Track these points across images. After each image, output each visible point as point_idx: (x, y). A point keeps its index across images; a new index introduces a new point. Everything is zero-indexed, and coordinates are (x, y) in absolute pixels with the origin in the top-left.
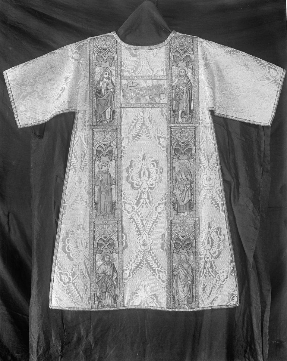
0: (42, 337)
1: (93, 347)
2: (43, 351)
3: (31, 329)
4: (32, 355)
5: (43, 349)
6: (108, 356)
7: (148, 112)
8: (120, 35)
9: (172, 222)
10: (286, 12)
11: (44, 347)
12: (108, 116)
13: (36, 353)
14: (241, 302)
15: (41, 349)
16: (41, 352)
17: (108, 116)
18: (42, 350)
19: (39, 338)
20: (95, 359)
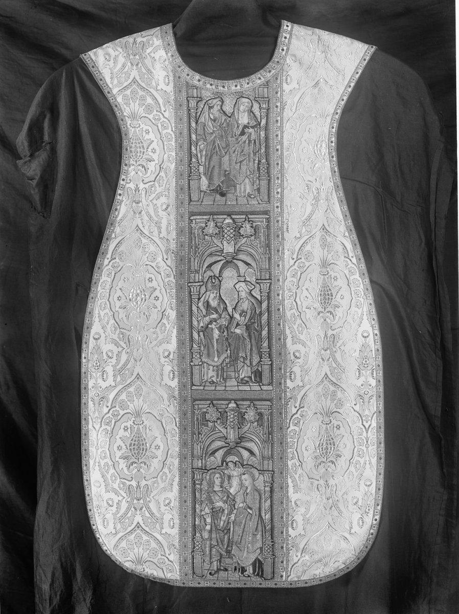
0: (59, 574)
1: (148, 587)
2: (60, 598)
3: (38, 560)
4: (40, 605)
5: (60, 595)
6: (176, 603)
7: (147, 55)
8: (177, 36)
9: (270, 360)
10: (457, 216)
11: (62, 591)
12: (375, 373)
13: (48, 601)
14: (450, 188)
15: (56, 595)
16: (56, 601)
17: (375, 373)
18: (58, 597)
19: (53, 575)
20: (153, 610)
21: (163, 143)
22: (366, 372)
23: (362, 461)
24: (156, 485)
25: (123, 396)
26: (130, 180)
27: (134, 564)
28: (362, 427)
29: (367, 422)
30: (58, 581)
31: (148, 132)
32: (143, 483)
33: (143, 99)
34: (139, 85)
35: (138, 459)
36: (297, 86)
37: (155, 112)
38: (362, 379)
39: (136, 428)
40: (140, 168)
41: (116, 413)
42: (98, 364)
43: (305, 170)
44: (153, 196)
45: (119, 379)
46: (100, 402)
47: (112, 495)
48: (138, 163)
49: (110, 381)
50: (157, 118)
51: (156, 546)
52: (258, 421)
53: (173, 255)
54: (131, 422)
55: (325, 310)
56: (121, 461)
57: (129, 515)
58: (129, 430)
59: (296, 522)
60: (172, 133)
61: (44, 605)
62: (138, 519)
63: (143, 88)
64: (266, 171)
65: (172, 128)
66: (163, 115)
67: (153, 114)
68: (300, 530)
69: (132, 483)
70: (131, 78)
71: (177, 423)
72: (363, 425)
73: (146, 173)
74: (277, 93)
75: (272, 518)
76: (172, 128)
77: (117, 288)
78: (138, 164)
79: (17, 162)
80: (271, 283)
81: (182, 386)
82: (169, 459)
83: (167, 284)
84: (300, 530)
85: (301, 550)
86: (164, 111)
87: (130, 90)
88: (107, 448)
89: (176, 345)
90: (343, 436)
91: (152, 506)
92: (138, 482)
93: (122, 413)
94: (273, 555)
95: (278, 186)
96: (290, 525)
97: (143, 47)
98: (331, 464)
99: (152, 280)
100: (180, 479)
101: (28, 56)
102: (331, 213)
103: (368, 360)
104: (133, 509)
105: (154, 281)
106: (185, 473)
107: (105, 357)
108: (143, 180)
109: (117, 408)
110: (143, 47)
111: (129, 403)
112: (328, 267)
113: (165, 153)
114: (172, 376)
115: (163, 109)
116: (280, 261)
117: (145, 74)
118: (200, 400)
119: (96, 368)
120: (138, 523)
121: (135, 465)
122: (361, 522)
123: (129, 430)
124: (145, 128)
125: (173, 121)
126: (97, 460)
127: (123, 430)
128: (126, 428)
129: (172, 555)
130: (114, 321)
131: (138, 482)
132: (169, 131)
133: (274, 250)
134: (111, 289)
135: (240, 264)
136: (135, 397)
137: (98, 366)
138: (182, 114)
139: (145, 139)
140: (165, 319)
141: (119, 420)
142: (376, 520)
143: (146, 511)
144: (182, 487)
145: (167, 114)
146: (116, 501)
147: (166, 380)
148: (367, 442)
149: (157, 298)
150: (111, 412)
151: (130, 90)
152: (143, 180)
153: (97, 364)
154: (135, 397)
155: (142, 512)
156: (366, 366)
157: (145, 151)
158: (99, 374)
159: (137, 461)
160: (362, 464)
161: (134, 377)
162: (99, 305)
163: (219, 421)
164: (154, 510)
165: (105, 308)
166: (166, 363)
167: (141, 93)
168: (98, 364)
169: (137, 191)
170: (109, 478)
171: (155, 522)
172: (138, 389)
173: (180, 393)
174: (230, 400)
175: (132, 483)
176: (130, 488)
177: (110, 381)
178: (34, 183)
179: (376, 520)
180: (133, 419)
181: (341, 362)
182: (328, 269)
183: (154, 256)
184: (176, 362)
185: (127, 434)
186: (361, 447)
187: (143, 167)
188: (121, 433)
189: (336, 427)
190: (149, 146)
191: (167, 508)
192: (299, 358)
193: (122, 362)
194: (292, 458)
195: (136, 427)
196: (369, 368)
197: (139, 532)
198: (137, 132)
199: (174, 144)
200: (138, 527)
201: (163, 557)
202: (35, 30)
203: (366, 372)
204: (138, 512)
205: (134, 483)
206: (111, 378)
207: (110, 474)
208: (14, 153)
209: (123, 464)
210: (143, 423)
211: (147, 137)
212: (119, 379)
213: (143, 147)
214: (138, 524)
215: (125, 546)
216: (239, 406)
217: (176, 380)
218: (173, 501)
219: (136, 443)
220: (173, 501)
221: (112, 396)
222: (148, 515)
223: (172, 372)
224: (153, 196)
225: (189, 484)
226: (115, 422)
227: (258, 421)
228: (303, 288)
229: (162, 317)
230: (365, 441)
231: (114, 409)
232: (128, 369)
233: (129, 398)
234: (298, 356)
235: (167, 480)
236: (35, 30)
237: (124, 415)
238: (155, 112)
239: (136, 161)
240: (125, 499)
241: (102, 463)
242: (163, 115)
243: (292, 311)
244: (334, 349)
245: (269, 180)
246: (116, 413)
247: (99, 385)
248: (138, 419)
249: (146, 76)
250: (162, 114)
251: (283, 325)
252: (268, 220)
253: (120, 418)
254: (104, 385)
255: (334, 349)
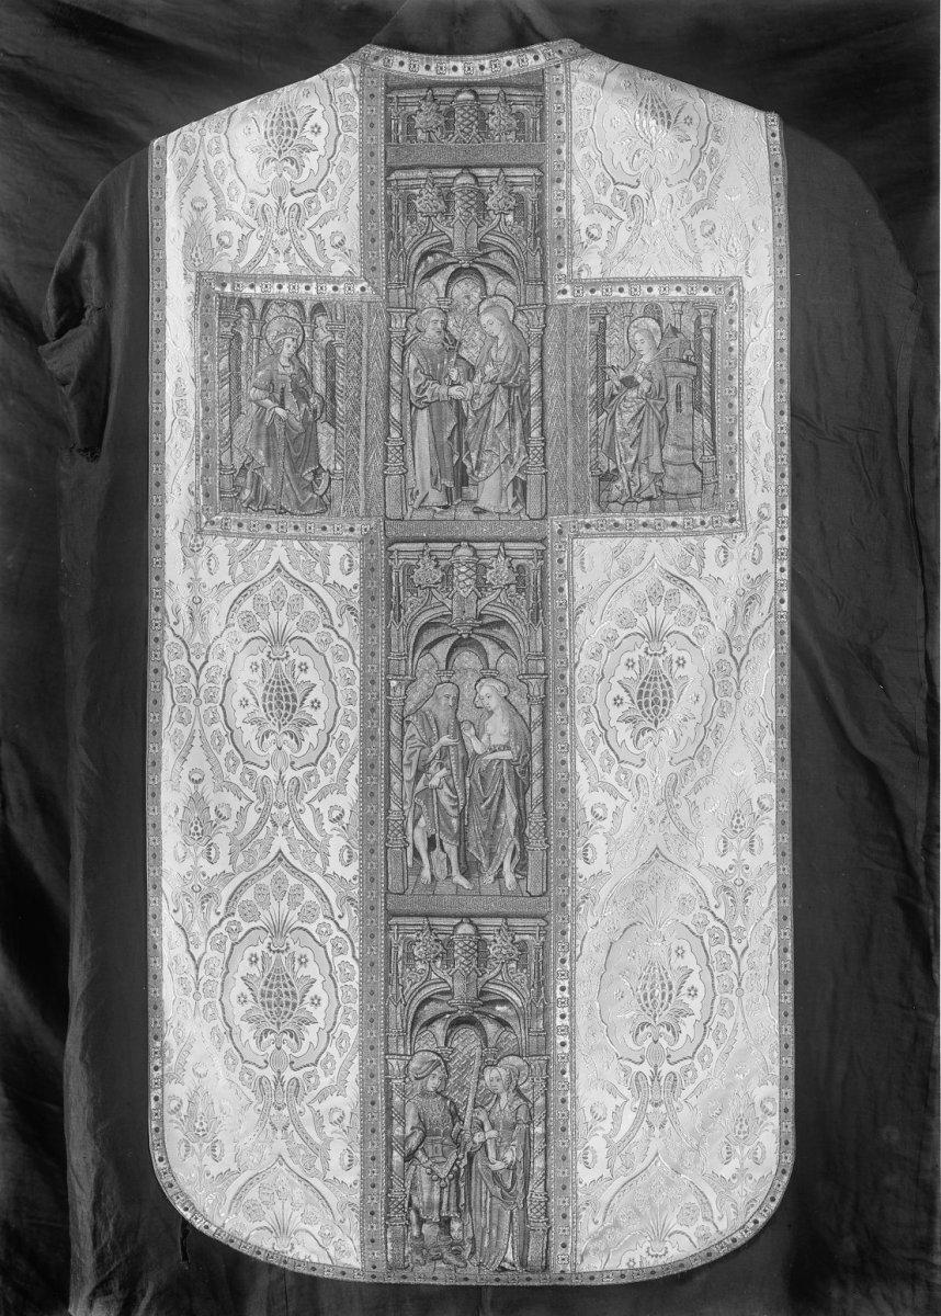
5: (115, 1225)
15: (107, 1225)
18: (111, 1229)
21: (335, 984)
22: (739, 842)
23: (729, 1024)
24: (313, 779)
25: (248, 895)
26: (268, 762)
27: (274, 1234)
28: (730, 951)
29: (739, 649)
30: (109, 1197)
31: (303, 962)
32: (289, 774)
33: (297, 892)
34: (288, 575)
35: (279, 1024)
36: (607, 1173)
37: (321, 919)
38: (731, 855)
39: (273, 959)
40: (286, 1036)
41: (234, 927)
42: (200, 831)
43: (616, 163)
44: (313, 793)
45: (239, 570)
46: (203, 903)
47: (229, 797)
48: (283, 156)
49: (223, 864)
50: (324, 929)
51: (314, 899)
52: (514, 210)
53: (354, 1213)
54: (264, 656)
55: (656, 725)
56: (245, 1026)
57: (262, 836)
58: (260, 962)
59: (594, 849)
60: (353, 962)
61: (82, 1245)
62: (280, 843)
63: (297, 583)
64: (543, 1211)
65: (354, 952)
66: (337, 633)
67: (318, 922)
68: (600, 864)
69: (266, 200)
70: (272, 563)
71: (357, 951)
72: (731, 947)
73: (300, 748)
74: (564, 933)
75: (544, 744)
76: (354, 952)
77: (238, 976)
78: (282, 1028)
79: (40, 348)
80: (548, 1060)
81: (368, 878)
82: (341, 155)
83: (337, 969)
84: (600, 864)
85: (603, 1210)
86: (340, 625)
87: (271, 876)
88: (218, 996)
89: (355, 798)
90: (691, 971)
91: (307, 818)
92: (280, 199)
93: (246, 927)
94: (544, 467)
95: (560, 576)
96: (580, 855)
97: (297, 790)
98: (665, 1030)
99: (307, 961)
100: (362, 197)
101: (61, 135)
102: (672, 824)
103: (746, 1123)
104: (269, 824)
105: (311, 964)
106: (373, 710)
107: (213, 817)
108: (293, 189)
109: (237, 917)
110: (297, 790)
111: (264, 1208)
112: (667, 1239)
113: (340, 134)
114: (346, 566)
115: (337, 912)
116: (566, 668)
117: (300, 1146)
118: (408, 915)
119: (196, 837)
120: (280, 851)
121: (272, 1036)
122: (722, 555)
123: (260, 962)
124: (299, 660)
125: (356, 936)
126: (202, 157)
127: (248, 962)
128: (253, 959)
129: (346, 918)
130: (230, 1045)
131: (280, 199)
132: (348, 958)
133: (556, 818)
134: (226, 684)
135: (489, 646)
136: (272, 896)
137: (198, 546)
138: (375, 229)
139: (299, 681)
140: (333, 1046)
141: (240, 941)
142: (756, 1222)
143: (295, 1133)
144: (367, 212)
145: (344, 632)
146: (236, 809)
147: (335, 866)
148: (740, 984)
149: (316, 704)
150: (224, 923)
151: (271, 876)
152: (293, 189)
153: (196, 829)
154: (272, 896)
155: (286, 1134)
156: (738, 830)
157: (298, 705)
158: (200, 849)
159: (274, 1027)
160: (729, 1031)
161: (271, 856)
162: (201, 1009)
163: (439, 586)
164: (311, 1131)
165: (213, 721)
166: (337, 259)
167: (293, 881)
168: (200, 831)
169: (281, 211)
170: (222, 762)
171: (313, 850)
172: (279, 881)
173: (363, 167)
174: (458, 541)
175: (266, 200)
176: (263, 1082)
177: (223, 864)
178: (67, 391)
179: (756, 1222)
180: (269, 940)
181: (688, 825)
182: (667, 1244)
183: (313, 911)
184: (354, 829)
185: (255, 970)
186: (726, 995)
187: (292, 735)
188: (243, 967)
189: (677, 662)
190: (307, 695)
191: (336, 825)
192: (596, 239)
193: (249, 826)
194: (587, 722)
195: (274, 956)
196: (745, 834)
197: (282, 870)
198: (284, 668)
199: (357, 987)
200: (280, 860)
201: (327, 630)
202: (76, 83)
203: (739, 842)
204: (280, 831)
205: (272, 774)
206: (224, 859)
207: (227, 184)
208: (31, 332)
209: (247, 1033)
210: (288, 948)
211: (303, 677)
212: (240, 860)
213: (294, 994)
214: (280, 856)
215: (250, 608)
216: (479, 553)
217: (355, 865)
218: (347, 812)
219: (274, 990)
220: (347, 812)
221: (226, 893)
222: (298, 1140)
223: (347, 1153)
224: (313, 793)
225: (381, 961)
226: (233, 945)
227: (514, 210)
228: (613, 681)
229: (327, 744)
230: (736, 983)
231: (230, 919)
232: (259, 842)
233: (267, 1198)
234: (596, 235)
235: (336, 772)
236: (76, 83)
237: (250, 931)
238: (321, 919)
239: (279, 1024)
240: (253, 805)
241: (208, 731)
242: (337, 633)
243: (588, 727)
244: (674, 800)
245: (545, 474)
246: (234, 927)
247: (202, 870)
248: (279, 941)
249: (302, 558)
250: (335, 631)
251: (571, 678)
252: (544, 931)
253: (243, 938)
254: (211, 870)
255: (674, 800)
